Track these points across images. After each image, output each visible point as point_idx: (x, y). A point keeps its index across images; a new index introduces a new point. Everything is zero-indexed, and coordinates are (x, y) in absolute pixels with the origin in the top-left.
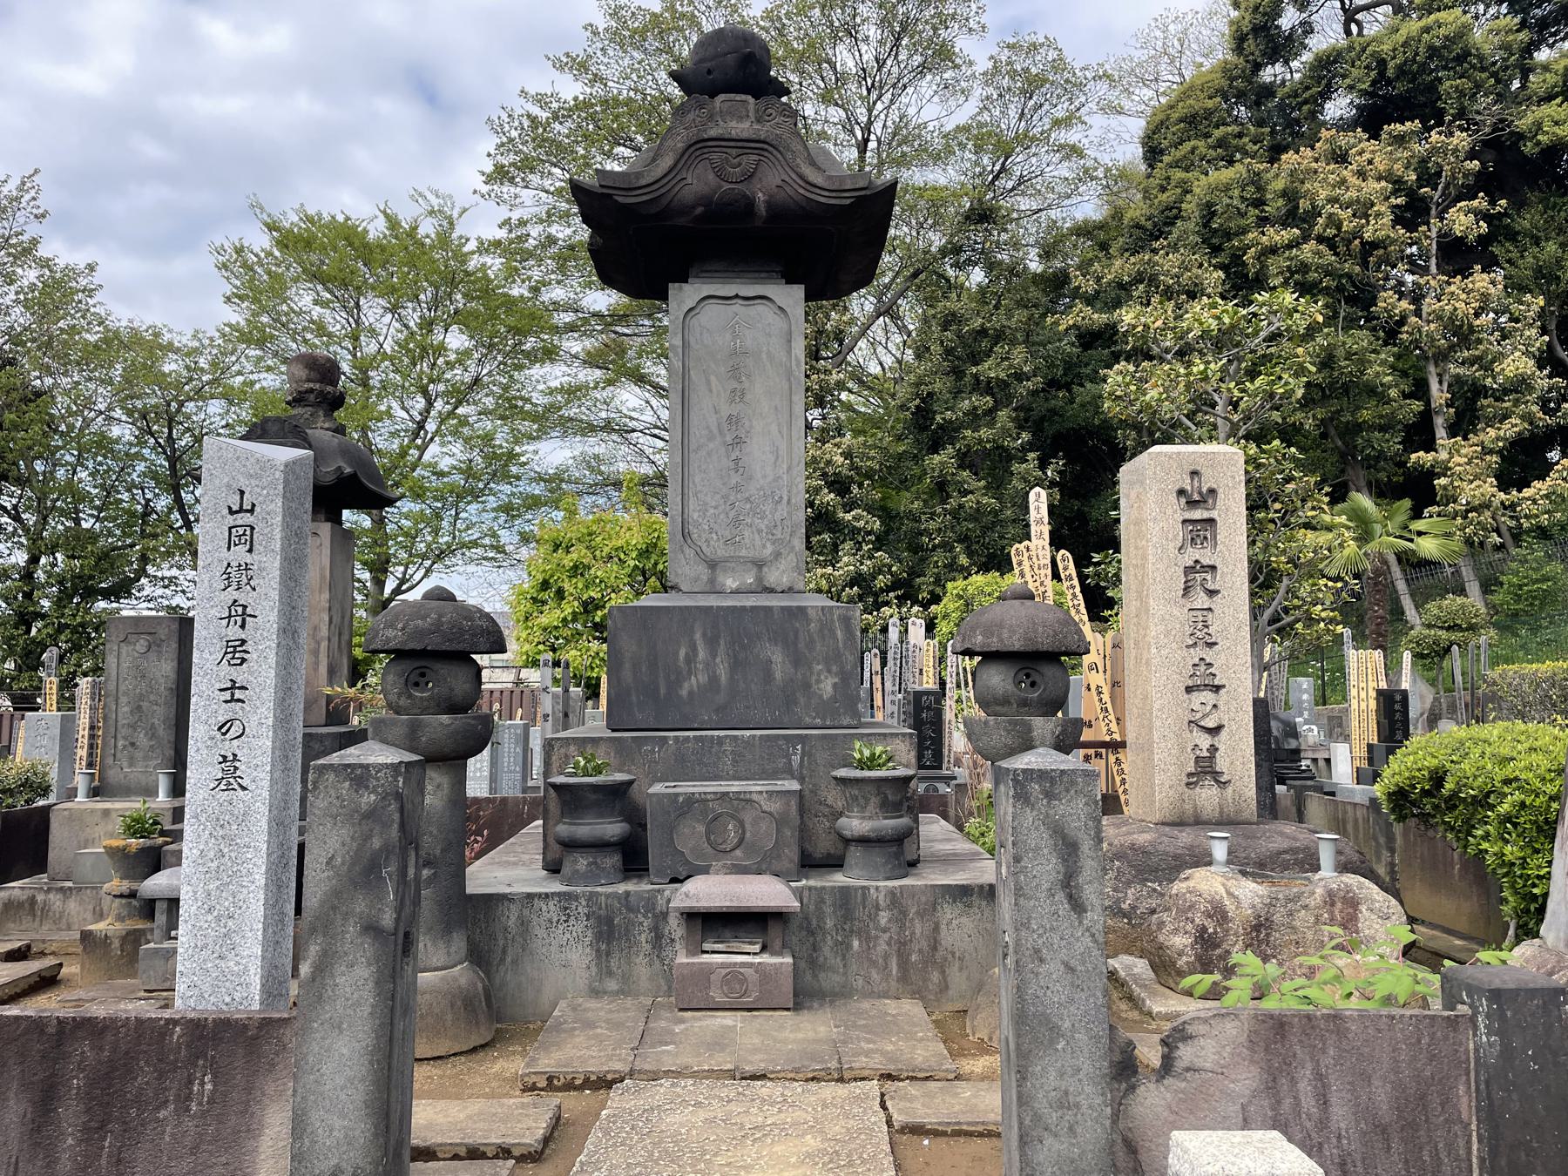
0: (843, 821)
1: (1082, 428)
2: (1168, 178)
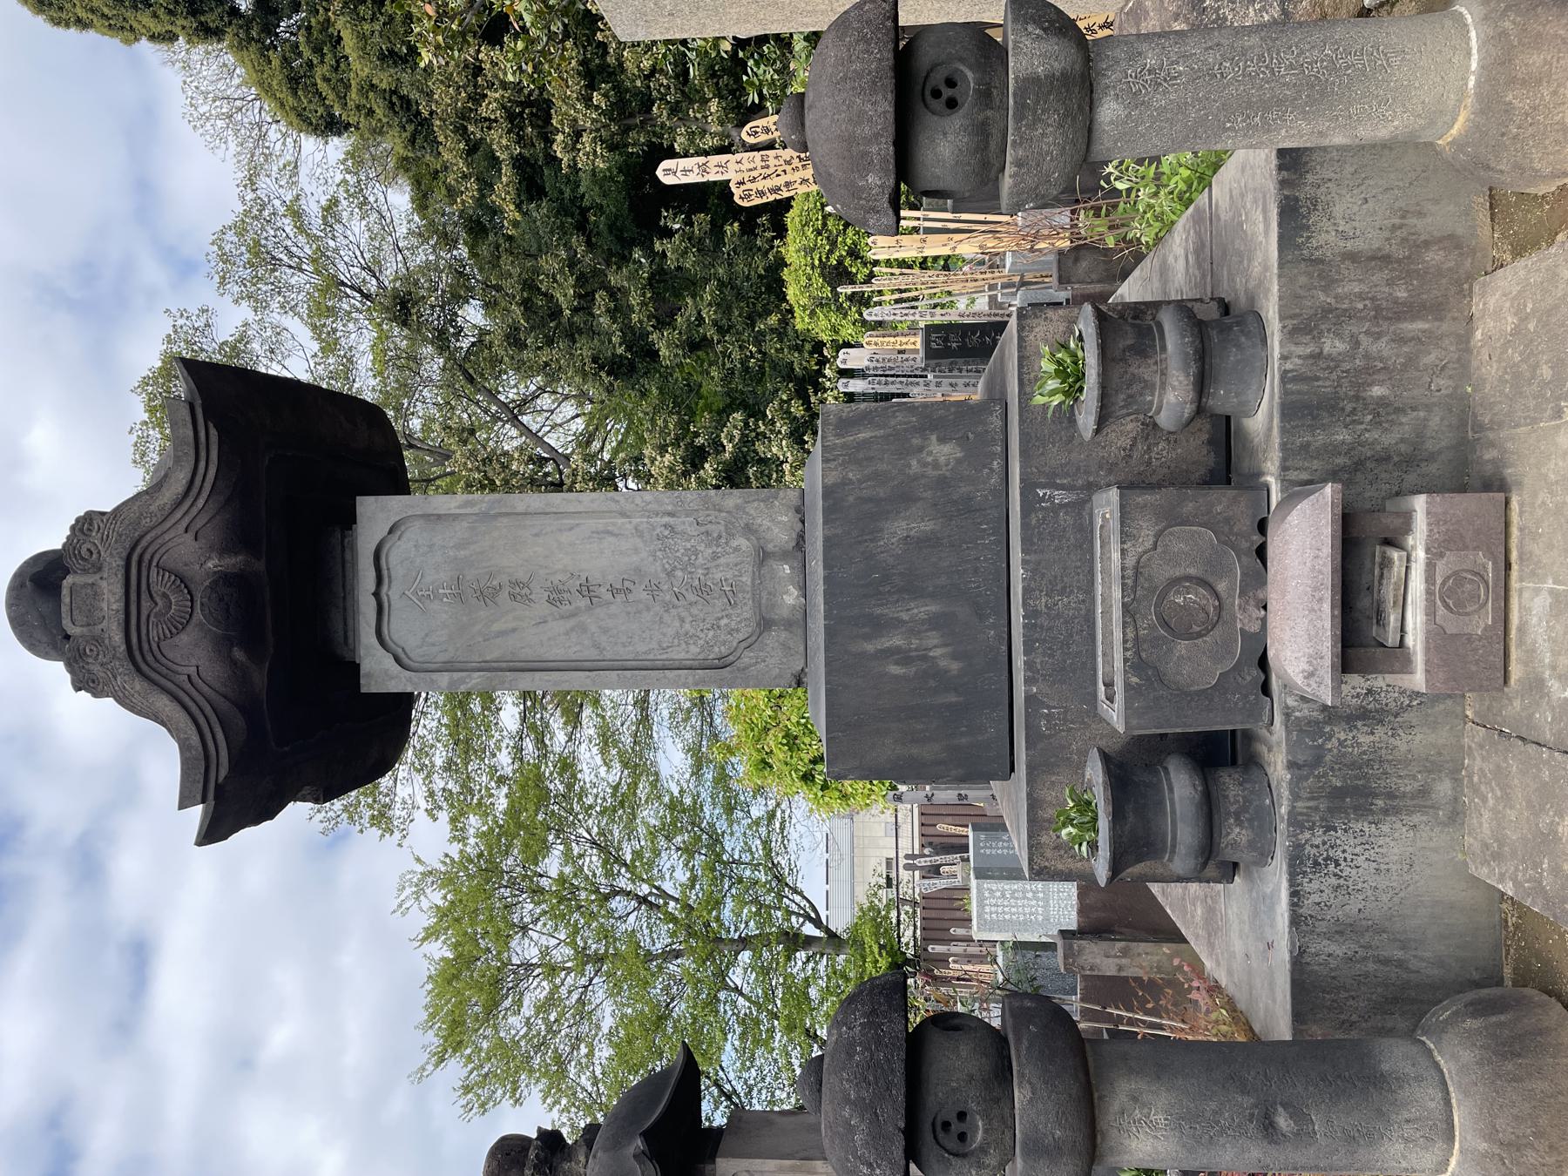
0: (1165, 419)
1: (628, 194)
2: (358, 107)
